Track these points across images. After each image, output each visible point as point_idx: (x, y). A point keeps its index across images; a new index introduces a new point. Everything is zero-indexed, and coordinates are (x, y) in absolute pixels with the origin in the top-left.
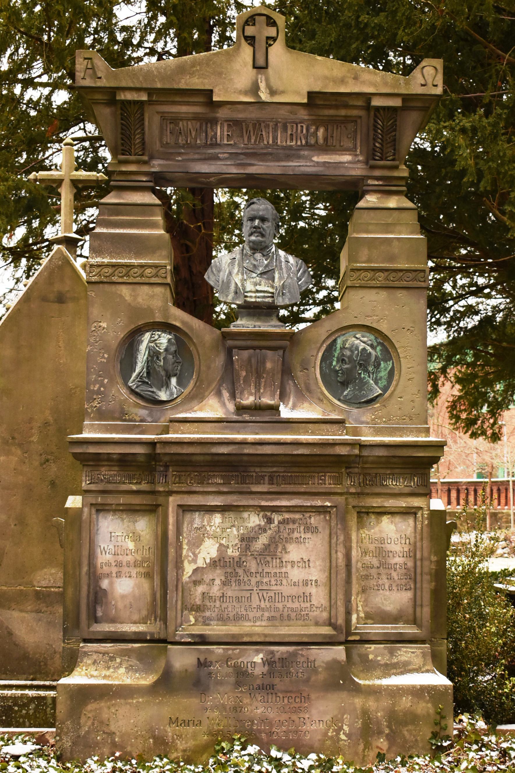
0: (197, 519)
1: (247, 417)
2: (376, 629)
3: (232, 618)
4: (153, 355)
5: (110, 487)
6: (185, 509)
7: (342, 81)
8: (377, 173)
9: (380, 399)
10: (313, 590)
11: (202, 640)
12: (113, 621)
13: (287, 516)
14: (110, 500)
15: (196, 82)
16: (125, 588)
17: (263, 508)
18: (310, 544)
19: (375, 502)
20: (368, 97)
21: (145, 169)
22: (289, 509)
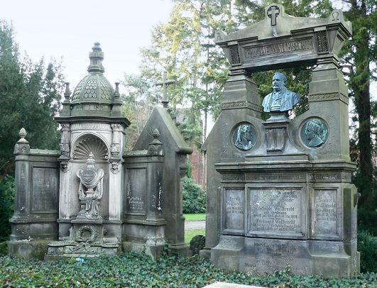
0: (254, 192)
1: (270, 154)
2: (321, 236)
3: (127, 244)
4: (242, 133)
5: (229, 181)
6: (251, 188)
7: (303, 24)
8: (322, 56)
9: (323, 145)
10: (295, 219)
11: (256, 237)
12: (231, 228)
13: (285, 191)
14: (229, 185)
15: (252, 35)
16: (235, 217)
17: (277, 188)
18: (294, 201)
19: (321, 185)
20: (312, 29)
21: (241, 67)
22: (286, 188)
